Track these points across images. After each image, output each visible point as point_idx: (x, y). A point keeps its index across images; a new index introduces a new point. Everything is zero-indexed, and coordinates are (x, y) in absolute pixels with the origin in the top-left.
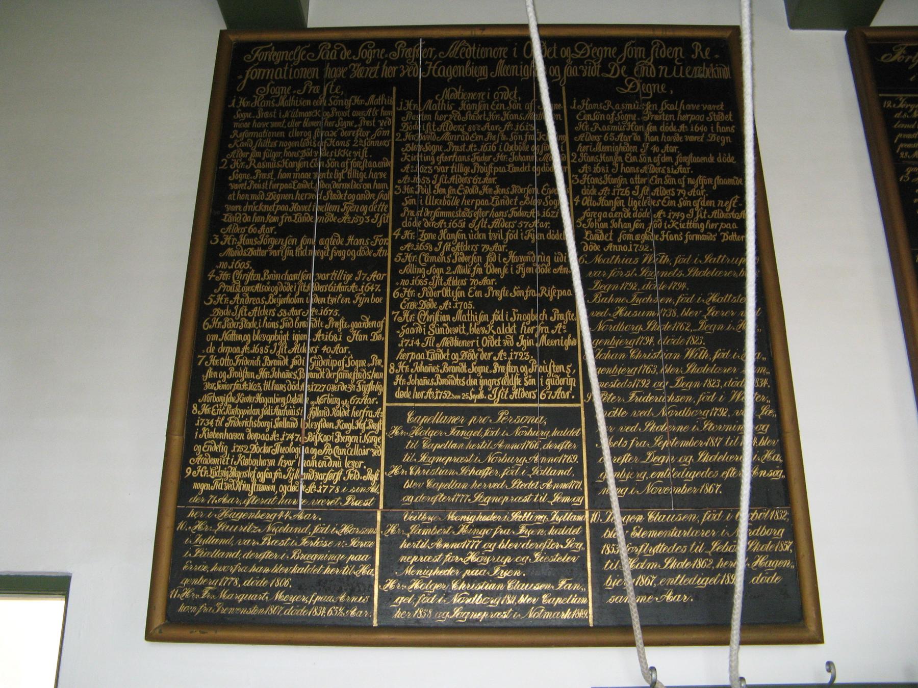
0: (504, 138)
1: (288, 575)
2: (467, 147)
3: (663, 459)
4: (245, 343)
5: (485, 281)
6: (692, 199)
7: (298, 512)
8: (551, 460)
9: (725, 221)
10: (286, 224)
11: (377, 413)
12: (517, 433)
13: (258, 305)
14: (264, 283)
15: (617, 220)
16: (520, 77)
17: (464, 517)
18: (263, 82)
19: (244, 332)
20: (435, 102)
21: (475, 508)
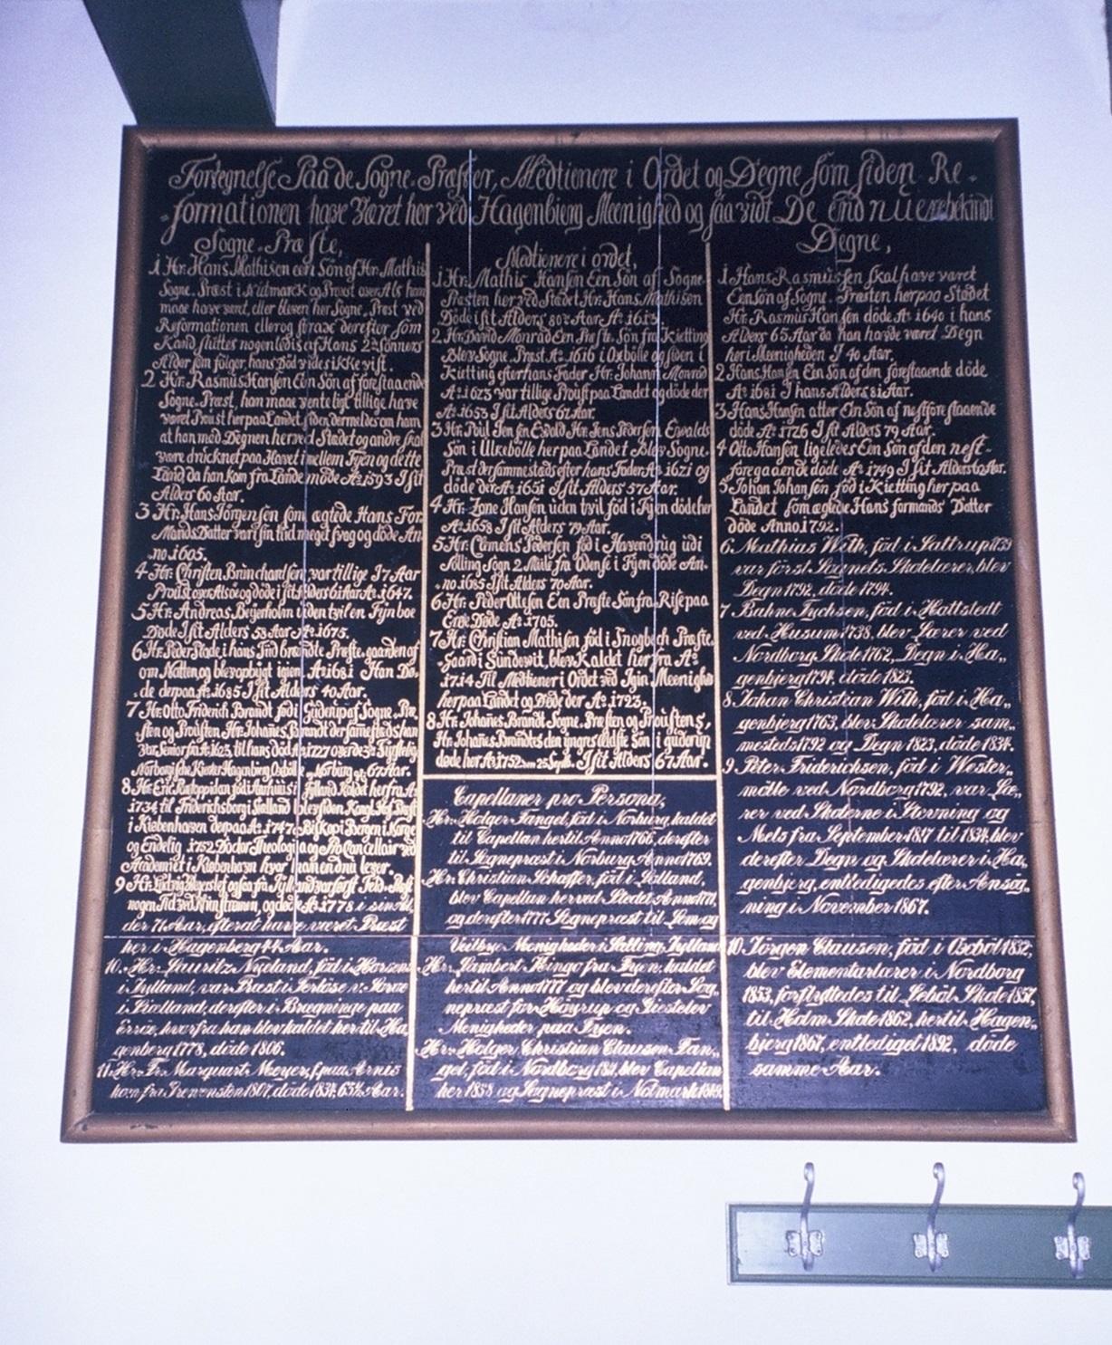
0: (607, 338)
1: (279, 1037)
2: (547, 355)
3: (841, 861)
4: (201, 681)
5: (575, 582)
6: (908, 441)
7: (291, 941)
8: (671, 861)
9: (960, 479)
10: (259, 486)
11: (410, 789)
12: (621, 819)
13: (220, 621)
14: (228, 584)
15: (784, 480)
16: (636, 225)
17: (540, 946)
18: (206, 229)
19: (200, 663)
20: (495, 272)
21: (557, 932)
